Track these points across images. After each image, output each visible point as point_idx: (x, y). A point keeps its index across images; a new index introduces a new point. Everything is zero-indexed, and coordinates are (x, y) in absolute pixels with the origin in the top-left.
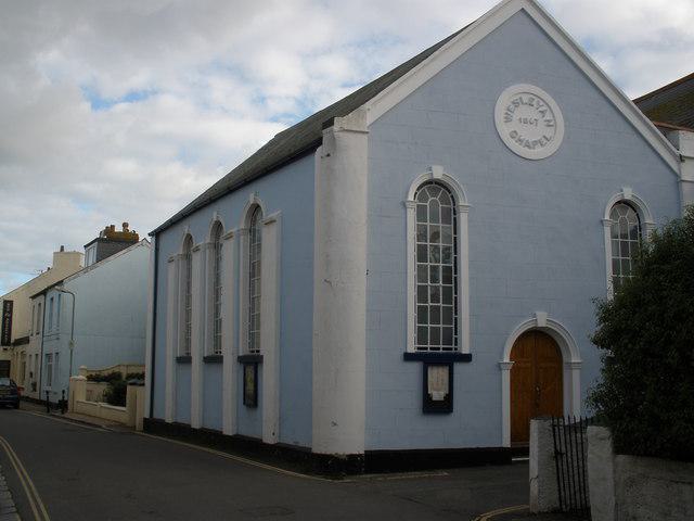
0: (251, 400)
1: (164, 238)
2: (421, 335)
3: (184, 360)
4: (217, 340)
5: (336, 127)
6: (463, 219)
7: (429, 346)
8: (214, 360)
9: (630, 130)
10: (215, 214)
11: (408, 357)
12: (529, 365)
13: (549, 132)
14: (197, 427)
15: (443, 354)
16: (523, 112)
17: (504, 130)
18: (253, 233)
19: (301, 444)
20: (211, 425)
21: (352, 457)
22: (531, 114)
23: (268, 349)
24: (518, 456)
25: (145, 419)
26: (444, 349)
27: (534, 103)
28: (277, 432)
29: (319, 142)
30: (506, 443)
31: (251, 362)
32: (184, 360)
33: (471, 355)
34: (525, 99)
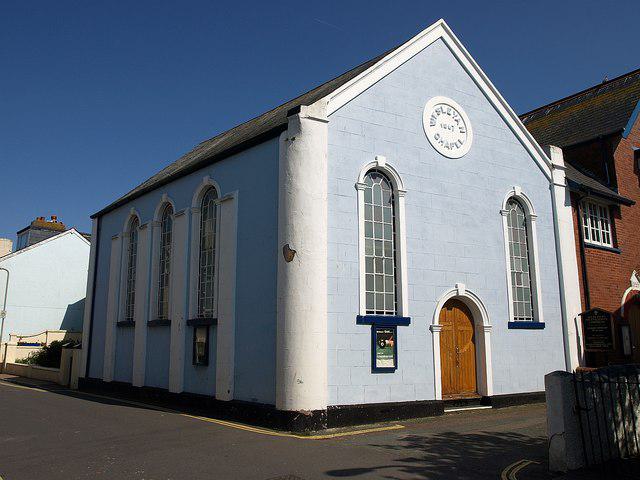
0: (202, 358)
1: (106, 220)
2: (369, 303)
3: (128, 324)
4: (130, 309)
5: (302, 114)
6: (402, 201)
7: (375, 310)
8: (161, 323)
9: (102, 232)
10: (164, 196)
11: (360, 320)
12: (450, 328)
13: (462, 137)
14: (109, 380)
15: (377, 317)
16: (442, 119)
17: (431, 133)
18: (166, 225)
19: (261, 400)
20: (156, 383)
21: (317, 413)
22: (448, 120)
23: (225, 310)
24: (450, 407)
25: (80, 379)
26: (377, 312)
27: (451, 113)
28: (232, 389)
29: (284, 127)
30: (439, 397)
31: (204, 324)
32: (128, 324)
33: (409, 319)
34: (445, 108)
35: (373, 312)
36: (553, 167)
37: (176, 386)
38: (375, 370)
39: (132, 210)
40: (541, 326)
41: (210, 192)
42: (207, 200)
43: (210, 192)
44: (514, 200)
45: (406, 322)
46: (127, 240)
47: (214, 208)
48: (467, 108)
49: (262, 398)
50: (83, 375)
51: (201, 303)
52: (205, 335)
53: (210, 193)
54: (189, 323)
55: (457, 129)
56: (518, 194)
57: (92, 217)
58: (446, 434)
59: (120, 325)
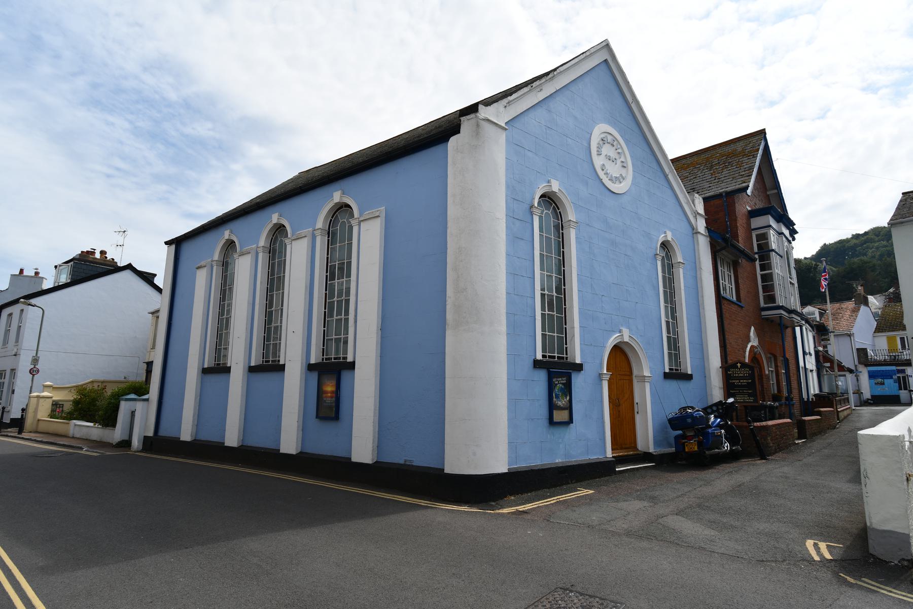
11: (537, 364)
13: (623, 172)
17: (598, 162)
20: (258, 441)
27: (615, 143)
30: (609, 454)
35: (554, 357)
36: (696, 214)
37: (289, 444)
38: (552, 422)
39: (226, 234)
40: (688, 377)
41: (279, 230)
42: (276, 238)
43: (279, 230)
44: (665, 245)
45: (579, 368)
46: (217, 271)
47: (283, 247)
48: (626, 141)
49: (421, 459)
50: (150, 433)
51: (266, 347)
52: (334, 382)
53: (230, 245)
54: (311, 367)
55: (619, 162)
56: (669, 239)
57: (166, 243)
58: (627, 501)
59: (205, 371)
